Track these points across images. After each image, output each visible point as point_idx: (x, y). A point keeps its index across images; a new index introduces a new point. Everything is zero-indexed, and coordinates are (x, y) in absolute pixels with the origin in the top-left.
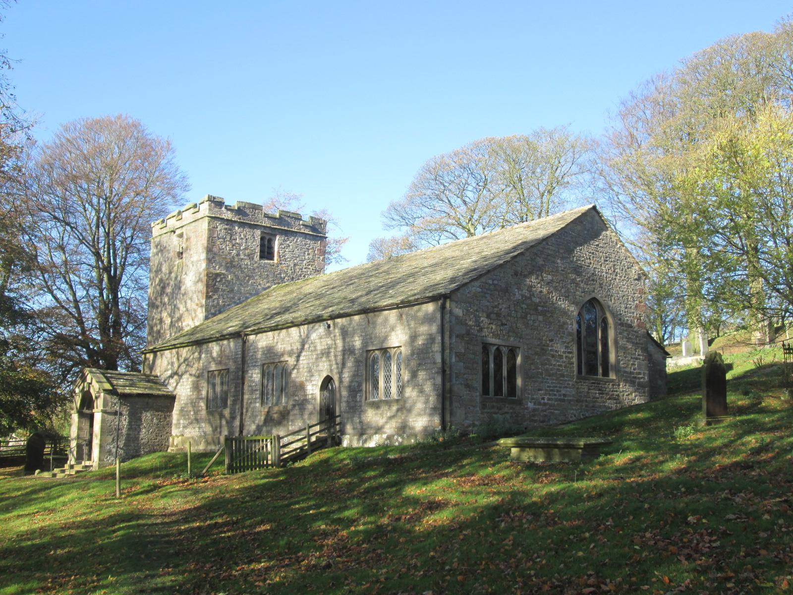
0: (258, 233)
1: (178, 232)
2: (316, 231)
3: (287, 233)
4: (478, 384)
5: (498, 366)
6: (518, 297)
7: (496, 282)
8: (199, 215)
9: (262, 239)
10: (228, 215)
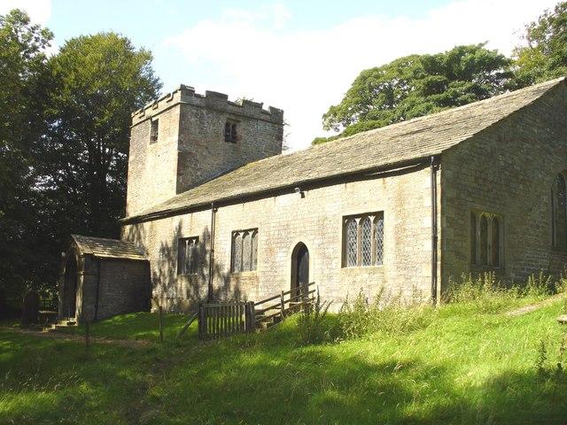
0: (223, 121)
1: (154, 119)
2: (276, 117)
3: (250, 118)
4: (468, 253)
5: (484, 232)
6: (502, 164)
7: (482, 146)
8: (172, 103)
9: (227, 125)
10: (197, 102)
